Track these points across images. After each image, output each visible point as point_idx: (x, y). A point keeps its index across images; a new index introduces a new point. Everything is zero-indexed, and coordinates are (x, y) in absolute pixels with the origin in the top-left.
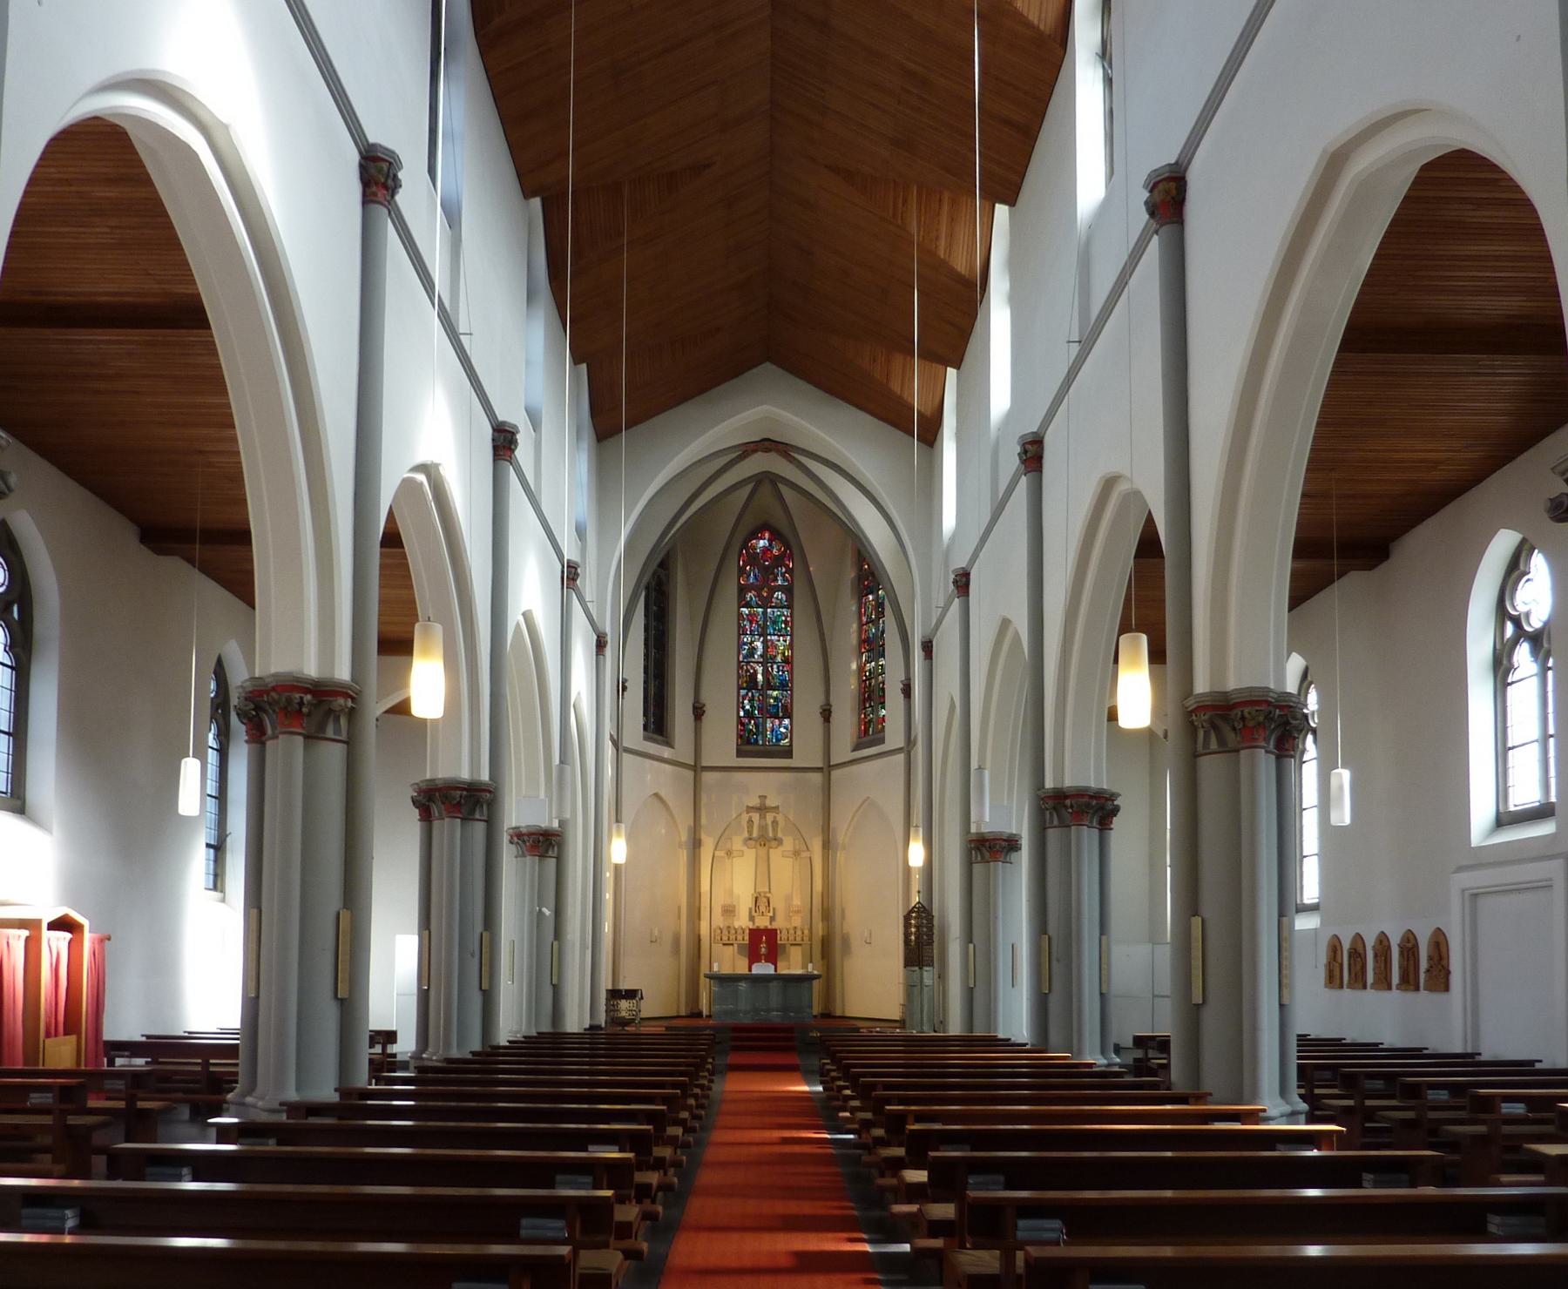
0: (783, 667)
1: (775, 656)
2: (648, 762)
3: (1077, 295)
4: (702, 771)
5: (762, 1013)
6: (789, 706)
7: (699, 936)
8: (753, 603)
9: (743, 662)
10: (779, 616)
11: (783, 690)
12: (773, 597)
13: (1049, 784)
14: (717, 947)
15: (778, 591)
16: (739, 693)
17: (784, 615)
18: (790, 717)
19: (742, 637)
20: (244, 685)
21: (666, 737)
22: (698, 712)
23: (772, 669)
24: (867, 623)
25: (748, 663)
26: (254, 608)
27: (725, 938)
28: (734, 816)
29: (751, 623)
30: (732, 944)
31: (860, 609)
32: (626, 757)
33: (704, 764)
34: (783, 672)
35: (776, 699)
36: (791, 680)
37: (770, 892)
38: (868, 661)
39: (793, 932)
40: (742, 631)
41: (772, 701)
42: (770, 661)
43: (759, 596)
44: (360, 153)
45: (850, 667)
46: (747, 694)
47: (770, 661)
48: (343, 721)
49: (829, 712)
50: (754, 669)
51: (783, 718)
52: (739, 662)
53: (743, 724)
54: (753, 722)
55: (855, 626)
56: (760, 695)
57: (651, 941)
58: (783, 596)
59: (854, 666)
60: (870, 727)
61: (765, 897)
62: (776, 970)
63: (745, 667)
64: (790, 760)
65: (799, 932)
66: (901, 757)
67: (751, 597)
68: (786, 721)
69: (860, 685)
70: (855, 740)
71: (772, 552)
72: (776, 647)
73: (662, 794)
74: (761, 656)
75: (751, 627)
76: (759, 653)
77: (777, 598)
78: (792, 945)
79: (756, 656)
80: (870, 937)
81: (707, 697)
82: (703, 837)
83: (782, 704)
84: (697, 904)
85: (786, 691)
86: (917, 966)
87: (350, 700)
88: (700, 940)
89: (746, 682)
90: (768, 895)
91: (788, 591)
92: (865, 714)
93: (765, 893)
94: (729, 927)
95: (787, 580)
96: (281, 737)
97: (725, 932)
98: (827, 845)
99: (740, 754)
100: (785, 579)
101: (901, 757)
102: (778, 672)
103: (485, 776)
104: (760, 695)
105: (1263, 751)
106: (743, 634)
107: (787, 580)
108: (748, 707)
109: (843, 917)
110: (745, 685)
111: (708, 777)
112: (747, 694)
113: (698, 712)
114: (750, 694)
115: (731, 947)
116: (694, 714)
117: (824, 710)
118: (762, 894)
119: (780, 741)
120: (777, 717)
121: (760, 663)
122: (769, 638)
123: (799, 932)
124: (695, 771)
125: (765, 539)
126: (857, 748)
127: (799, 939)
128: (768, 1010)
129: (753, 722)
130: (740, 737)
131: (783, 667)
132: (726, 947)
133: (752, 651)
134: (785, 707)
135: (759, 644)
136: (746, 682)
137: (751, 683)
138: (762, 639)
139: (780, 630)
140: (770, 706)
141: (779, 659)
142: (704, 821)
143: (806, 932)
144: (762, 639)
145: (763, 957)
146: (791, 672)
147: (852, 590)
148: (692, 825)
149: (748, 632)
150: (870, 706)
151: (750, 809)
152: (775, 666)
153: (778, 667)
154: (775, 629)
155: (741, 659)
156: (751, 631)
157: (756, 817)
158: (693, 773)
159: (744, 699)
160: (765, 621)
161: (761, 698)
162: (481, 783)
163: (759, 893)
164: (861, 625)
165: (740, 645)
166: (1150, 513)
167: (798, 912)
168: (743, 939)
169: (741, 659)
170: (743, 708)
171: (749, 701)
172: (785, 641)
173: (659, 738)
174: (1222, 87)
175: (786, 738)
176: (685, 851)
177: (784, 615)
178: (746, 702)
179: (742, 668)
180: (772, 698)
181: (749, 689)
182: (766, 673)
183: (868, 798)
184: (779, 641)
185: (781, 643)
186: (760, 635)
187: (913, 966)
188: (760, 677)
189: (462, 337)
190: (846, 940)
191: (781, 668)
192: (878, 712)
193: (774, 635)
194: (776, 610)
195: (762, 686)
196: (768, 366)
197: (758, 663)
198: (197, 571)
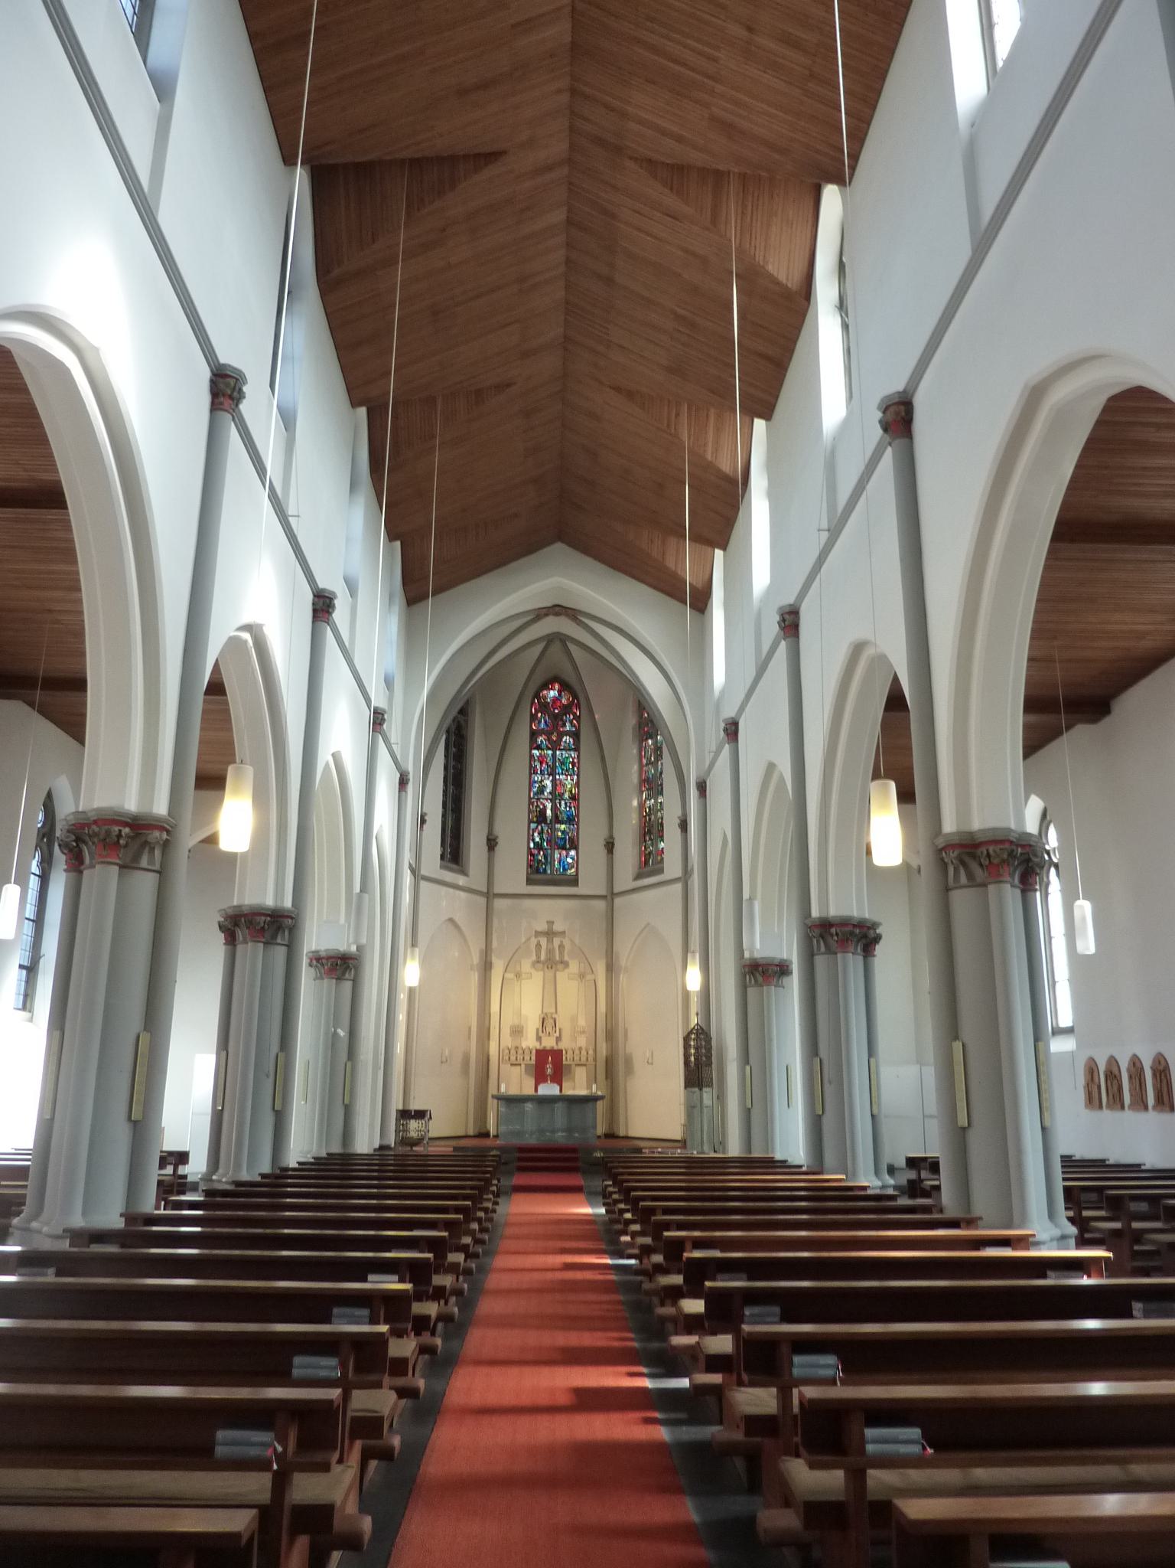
0: (570, 803)
1: (563, 794)
2: (444, 889)
4: (493, 898)
8: (544, 746)
10: (567, 758)
13: (815, 913)
18: (576, 848)
20: (68, 818)
22: (492, 843)
23: (560, 805)
26: (82, 742)
27: (513, 1058)
28: (523, 940)
29: (541, 763)
30: (520, 1065)
32: (423, 884)
34: (570, 808)
35: (563, 832)
36: (578, 815)
37: (556, 1012)
40: (533, 771)
41: (560, 834)
44: (212, 371)
45: (631, 801)
46: (537, 827)
48: (157, 853)
51: (570, 849)
52: (530, 798)
53: (532, 855)
54: (542, 853)
55: (636, 767)
57: (442, 1062)
59: (635, 803)
60: (650, 857)
62: (561, 1090)
63: (535, 804)
65: (584, 1052)
66: (678, 887)
67: (542, 741)
68: (573, 853)
70: (636, 870)
72: (564, 785)
73: (457, 919)
75: (541, 768)
76: (548, 791)
77: (565, 742)
79: (546, 794)
81: (499, 830)
82: (494, 959)
83: (569, 837)
86: (696, 1086)
87: (165, 833)
91: (576, 735)
93: (552, 1014)
94: (517, 1048)
96: (97, 866)
97: (513, 1052)
99: (530, 881)
101: (678, 887)
102: (566, 808)
103: (288, 903)
105: (1009, 885)
107: (575, 726)
108: (537, 839)
111: (499, 904)
112: (537, 827)
113: (492, 843)
114: (540, 828)
115: (519, 1067)
118: (549, 1016)
120: (563, 848)
123: (584, 1052)
126: (639, 876)
127: (584, 1059)
128: (553, 1131)
129: (542, 853)
130: (530, 866)
132: (513, 1068)
133: (542, 789)
135: (548, 783)
141: (566, 796)
142: (495, 944)
146: (577, 808)
149: (539, 772)
151: (538, 934)
152: (563, 803)
153: (566, 804)
154: (563, 770)
155: (532, 795)
159: (534, 831)
162: (284, 910)
164: (641, 766)
165: (531, 784)
166: (895, 674)
167: (583, 1032)
169: (532, 795)
170: (533, 840)
171: (539, 834)
173: (454, 866)
175: (573, 867)
176: (476, 974)
179: (533, 804)
181: (539, 823)
182: (554, 809)
185: (569, 782)
188: (549, 813)
189: (290, 519)
190: (629, 1061)
191: (568, 804)
194: (564, 752)
196: (559, 547)
197: (547, 799)
198: (36, 712)
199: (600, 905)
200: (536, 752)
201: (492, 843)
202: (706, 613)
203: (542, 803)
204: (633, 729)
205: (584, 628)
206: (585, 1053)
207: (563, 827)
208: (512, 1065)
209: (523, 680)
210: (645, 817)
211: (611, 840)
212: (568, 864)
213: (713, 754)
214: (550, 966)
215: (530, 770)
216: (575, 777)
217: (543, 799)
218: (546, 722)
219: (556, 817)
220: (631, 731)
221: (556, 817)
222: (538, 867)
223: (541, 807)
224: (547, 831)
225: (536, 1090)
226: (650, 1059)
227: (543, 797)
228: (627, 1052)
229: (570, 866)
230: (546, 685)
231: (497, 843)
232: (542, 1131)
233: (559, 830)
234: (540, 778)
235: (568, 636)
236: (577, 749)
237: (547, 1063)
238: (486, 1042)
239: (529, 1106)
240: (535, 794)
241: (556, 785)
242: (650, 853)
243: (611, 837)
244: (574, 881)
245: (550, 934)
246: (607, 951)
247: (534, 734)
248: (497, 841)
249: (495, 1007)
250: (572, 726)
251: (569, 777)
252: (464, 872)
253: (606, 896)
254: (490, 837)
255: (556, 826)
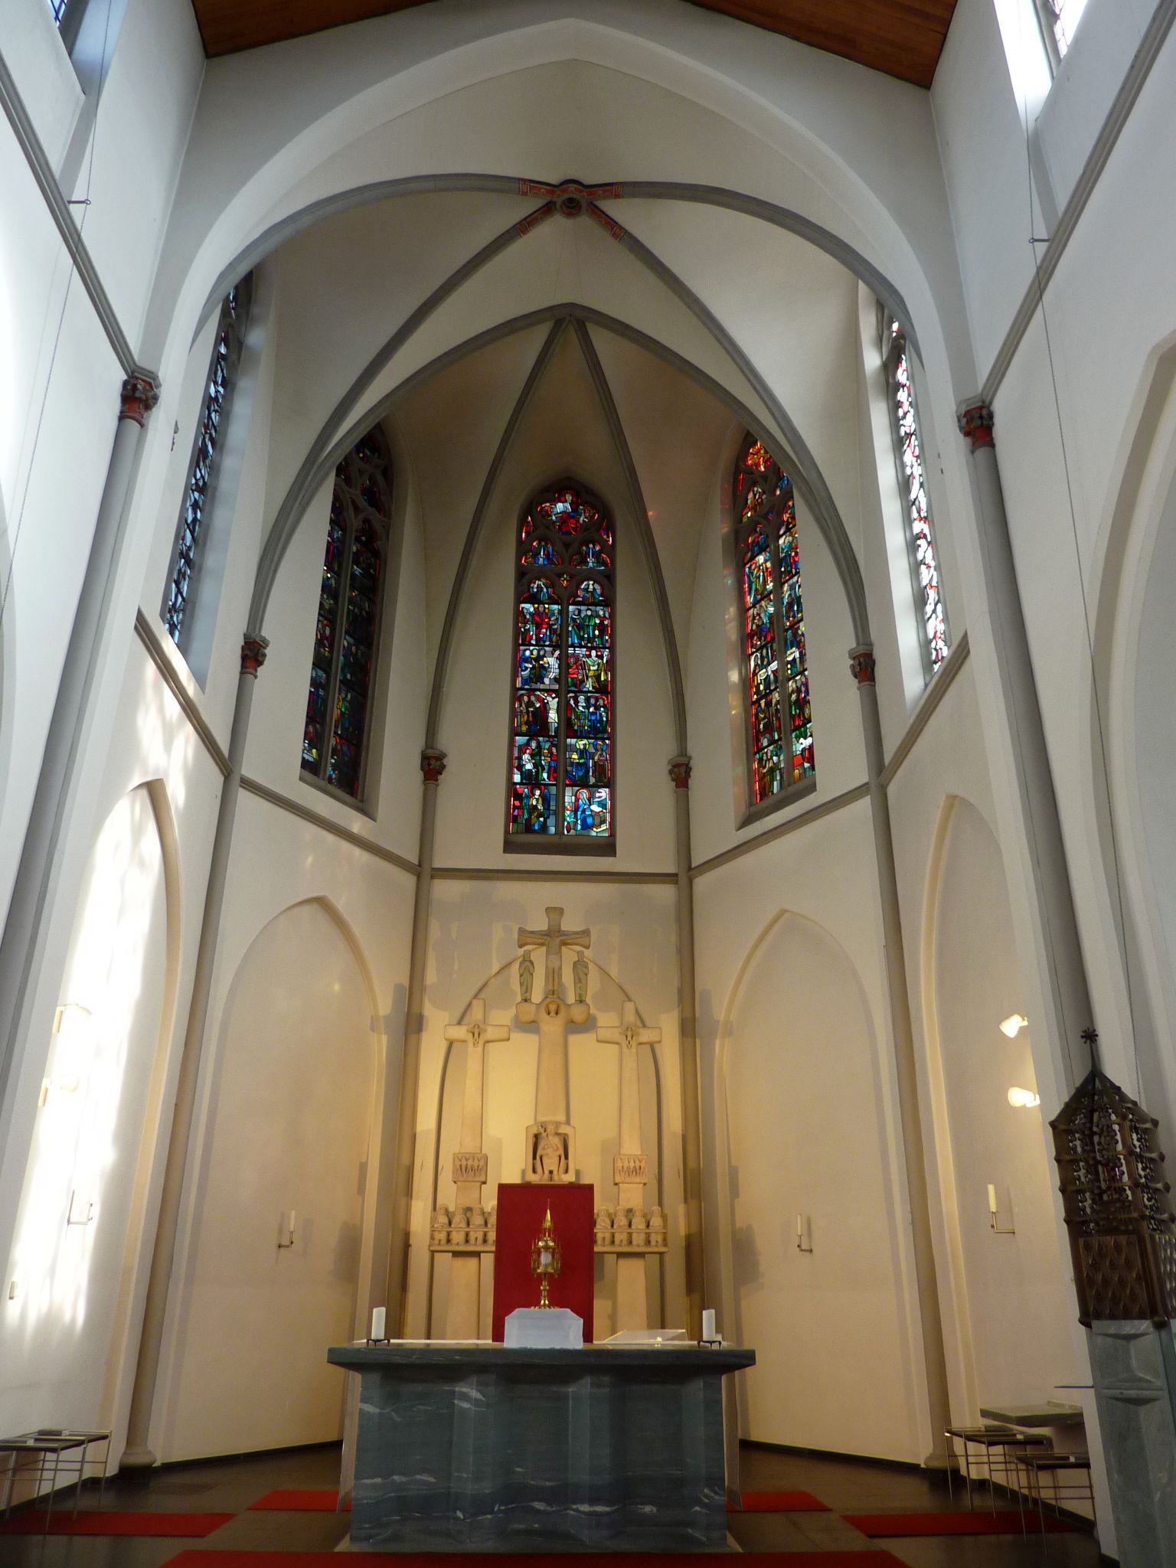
0: (597, 699)
1: (582, 681)
2: (310, 830)
3: (1035, 198)
4: (432, 877)
5: (540, 1506)
6: (608, 765)
7: (407, 1235)
8: (543, 596)
9: (522, 689)
10: (590, 617)
11: (596, 739)
12: (578, 587)
14: (443, 1260)
15: (588, 580)
16: (512, 743)
17: (598, 616)
18: (610, 784)
19: (522, 648)
21: (362, 801)
22: (432, 766)
23: (577, 702)
24: (756, 603)
25: (531, 691)
27: (458, 1237)
28: (495, 968)
29: (539, 627)
30: (477, 1254)
31: (740, 583)
32: (245, 800)
33: (438, 864)
34: (597, 708)
35: (583, 753)
36: (612, 721)
37: (568, 1122)
38: (760, 666)
39: (624, 1222)
40: (521, 639)
41: (575, 756)
42: (573, 689)
43: (551, 585)
45: (727, 677)
46: (528, 744)
47: (573, 689)
49: (688, 770)
50: (541, 700)
51: (597, 786)
52: (515, 689)
53: (518, 796)
54: (538, 792)
55: (732, 611)
56: (553, 745)
57: (280, 1246)
58: (597, 586)
59: (734, 676)
60: (773, 780)
61: (557, 1134)
62: (588, 1336)
63: (526, 698)
64: (611, 859)
65: (639, 1223)
66: (864, 807)
67: (539, 587)
68: (603, 793)
69: (747, 711)
70: (743, 809)
71: (578, 521)
72: (584, 666)
73: (341, 904)
74: (556, 680)
75: (537, 635)
76: (552, 675)
77: (586, 590)
78: (621, 1255)
79: (547, 681)
80: (810, 1236)
81: (448, 741)
82: (429, 1010)
83: (595, 764)
84: (405, 1160)
85: (603, 740)
86: (1142, 1316)
88: (407, 1246)
89: (526, 723)
90: (564, 1129)
91: (608, 579)
92: (761, 760)
93: (558, 1124)
94: (469, 1209)
95: (604, 564)
97: (459, 1220)
98: (689, 1029)
99: (509, 847)
100: (600, 562)
101: (864, 807)
102: (588, 707)
104: (553, 745)
106: (523, 644)
107: (604, 564)
108: (529, 766)
109: (734, 1190)
110: (524, 728)
111: (444, 890)
112: (528, 744)
113: (432, 766)
114: (534, 745)
115: (472, 1262)
116: (422, 768)
117: (676, 766)
118: (551, 1128)
119: (591, 827)
120: (583, 784)
121: (554, 691)
122: (571, 651)
123: (639, 1223)
124: (419, 876)
125: (566, 501)
126: (745, 822)
127: (638, 1239)
128: (563, 1495)
129: (538, 792)
130: (511, 819)
131: (597, 699)
132: (460, 1262)
133: (540, 672)
134: (599, 769)
135: (552, 661)
136: (526, 723)
137: (537, 724)
138: (557, 653)
139: (589, 640)
140: (572, 764)
141: (589, 685)
142: (431, 977)
143: (656, 1222)
144: (557, 653)
145: (544, 1286)
146: (611, 708)
147: (724, 550)
148: (406, 983)
149: (533, 642)
150: (772, 742)
151: (525, 937)
152: (581, 698)
153: (587, 700)
154: (581, 638)
155: (519, 684)
156: (538, 640)
157: (539, 955)
158: (415, 878)
159: (522, 749)
160: (564, 625)
161: (554, 750)
163: (544, 1126)
164: (743, 610)
165: (518, 662)
167: (637, 1171)
168: (485, 1241)
169: (519, 684)
170: (520, 767)
171: (532, 756)
172: (601, 657)
173: (347, 797)
174: (1003, 361)
175: (603, 822)
176: (384, 1038)
177: (598, 616)
178: (526, 757)
179: (520, 699)
180: (577, 751)
181: (532, 735)
182: (565, 709)
183: (783, 912)
184: (589, 656)
185: (593, 662)
186: (555, 647)
187: (1127, 1315)
188: (553, 716)
189: (72, 207)
190: (744, 1248)
191: (593, 701)
192: (790, 744)
193: (581, 646)
194: (583, 608)
195: (557, 730)
197: (549, 691)
199: (665, 894)
200: (529, 607)
201: (433, 762)
202: (931, 89)
203: (539, 699)
204: (724, 541)
205: (634, 196)
206: (642, 1226)
207: (581, 744)
208: (457, 1254)
209: (496, 443)
210: (758, 700)
211: (683, 760)
212: (594, 815)
213: (1045, 245)
214: (553, 1008)
215: (516, 640)
216: (606, 653)
217: (540, 690)
218: (547, 555)
219: (569, 724)
220: (720, 544)
221: (569, 724)
222: (528, 820)
223: (538, 705)
224: (550, 750)
225: (498, 1334)
226: (805, 1241)
227: (542, 686)
228: (738, 1225)
229: (597, 821)
230: (555, 489)
231: (443, 767)
232: (515, 1495)
233: (573, 749)
234: (535, 652)
235: (590, 310)
236: (608, 602)
237: (537, 1232)
238: (403, 1201)
239: (469, 1394)
240: (525, 681)
241: (568, 666)
242: (772, 770)
243: (683, 751)
244: (607, 847)
245: (554, 938)
246: (680, 991)
247: (523, 576)
248: (445, 761)
249: (426, 1121)
250: (598, 562)
251: (594, 653)
252: (365, 808)
253: (676, 875)
254: (430, 752)
255: (569, 740)
